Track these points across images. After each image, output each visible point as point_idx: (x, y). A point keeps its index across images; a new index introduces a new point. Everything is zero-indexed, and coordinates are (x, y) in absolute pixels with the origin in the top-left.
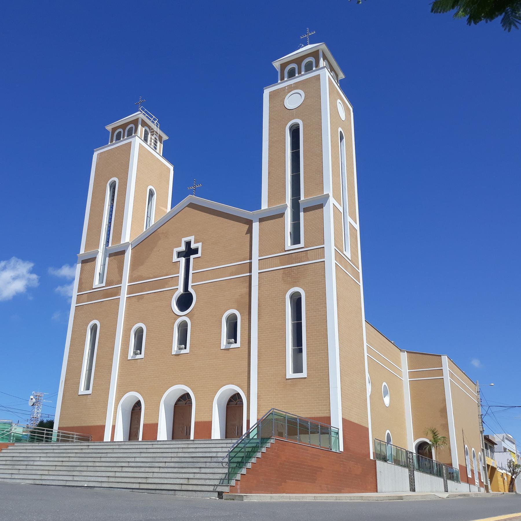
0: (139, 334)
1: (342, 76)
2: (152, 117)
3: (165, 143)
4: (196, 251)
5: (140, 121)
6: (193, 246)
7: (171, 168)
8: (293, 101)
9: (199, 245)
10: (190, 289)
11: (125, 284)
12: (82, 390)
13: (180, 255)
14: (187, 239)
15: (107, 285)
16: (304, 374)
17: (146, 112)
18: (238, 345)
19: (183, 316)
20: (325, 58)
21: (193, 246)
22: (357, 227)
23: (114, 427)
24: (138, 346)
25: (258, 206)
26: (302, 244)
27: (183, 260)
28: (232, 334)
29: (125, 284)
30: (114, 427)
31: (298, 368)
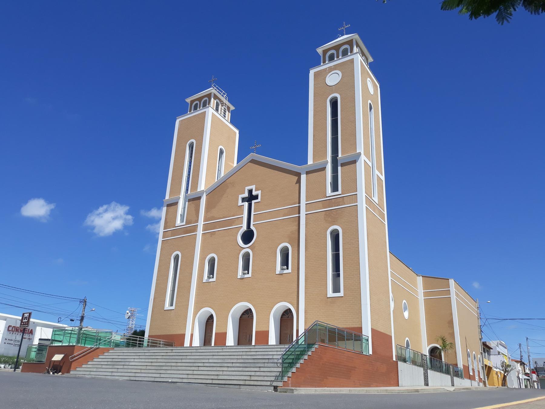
0: (212, 262)
1: (371, 60)
2: (222, 92)
3: (232, 113)
4: (256, 197)
5: (213, 95)
6: (254, 193)
7: (237, 132)
8: (333, 79)
9: (259, 193)
10: (252, 227)
11: (201, 223)
12: (167, 306)
13: (244, 200)
14: (249, 188)
15: (187, 224)
16: (341, 294)
17: (217, 88)
18: (290, 270)
19: (247, 248)
20: (358, 46)
21: (254, 193)
22: (383, 178)
23: (192, 335)
24: (211, 272)
25: (306, 162)
26: (340, 192)
27: (246, 204)
28: (285, 262)
29: (201, 223)
30: (192, 335)
31: (336, 289)
